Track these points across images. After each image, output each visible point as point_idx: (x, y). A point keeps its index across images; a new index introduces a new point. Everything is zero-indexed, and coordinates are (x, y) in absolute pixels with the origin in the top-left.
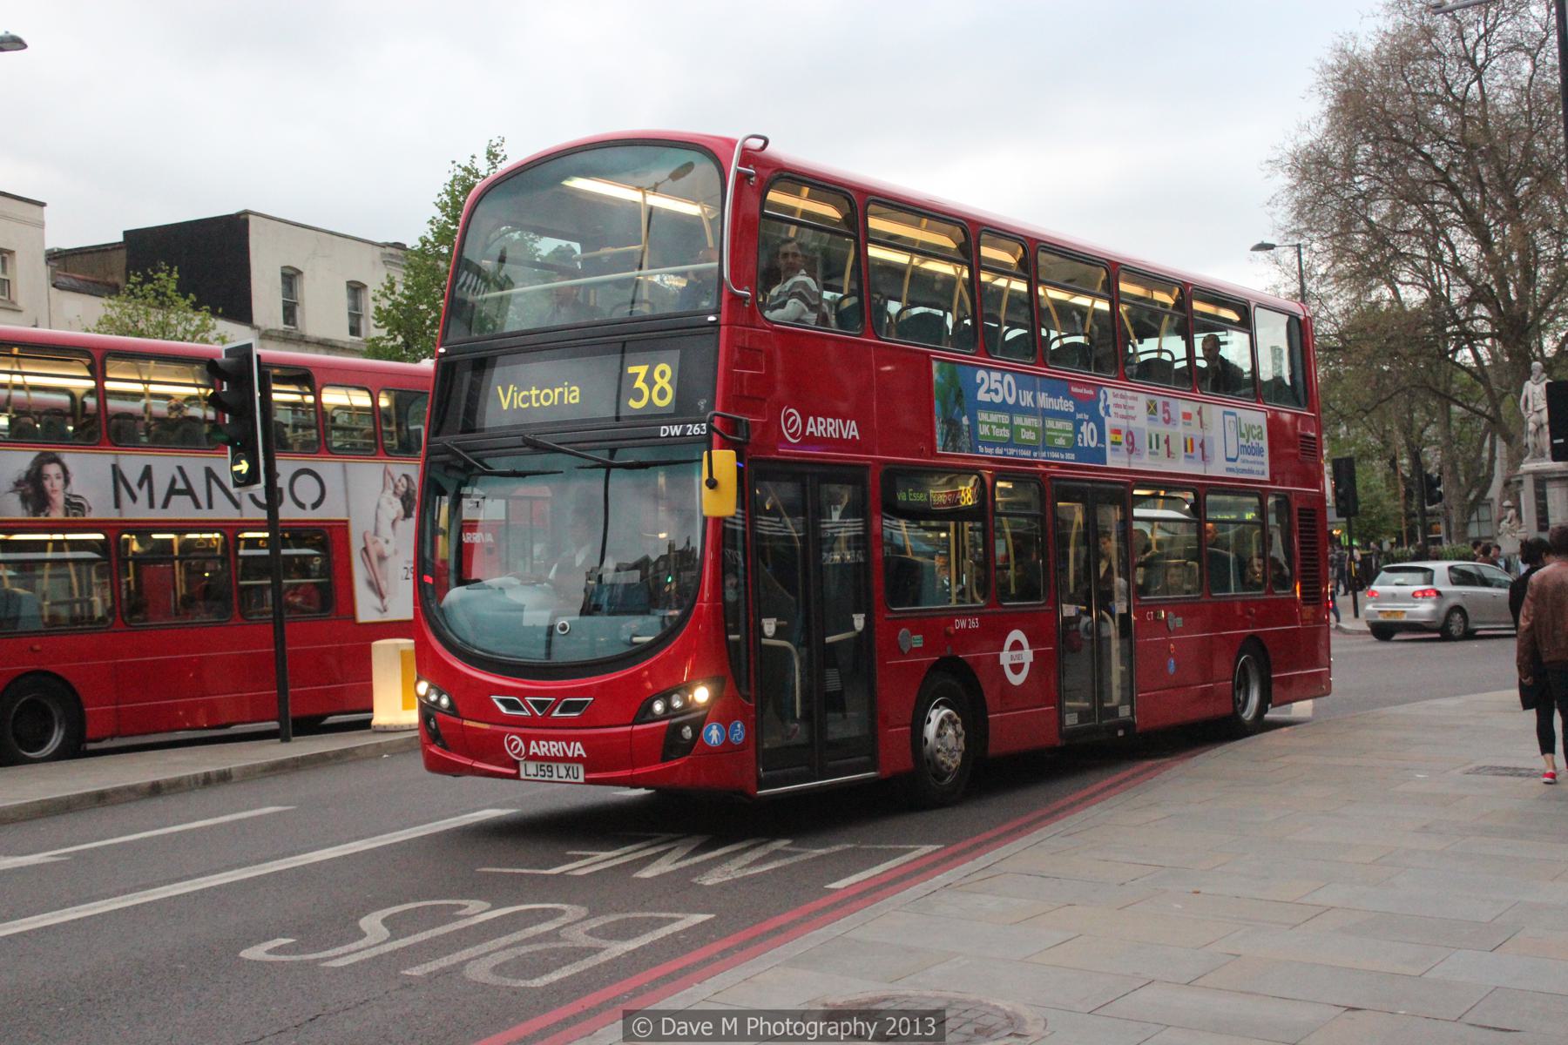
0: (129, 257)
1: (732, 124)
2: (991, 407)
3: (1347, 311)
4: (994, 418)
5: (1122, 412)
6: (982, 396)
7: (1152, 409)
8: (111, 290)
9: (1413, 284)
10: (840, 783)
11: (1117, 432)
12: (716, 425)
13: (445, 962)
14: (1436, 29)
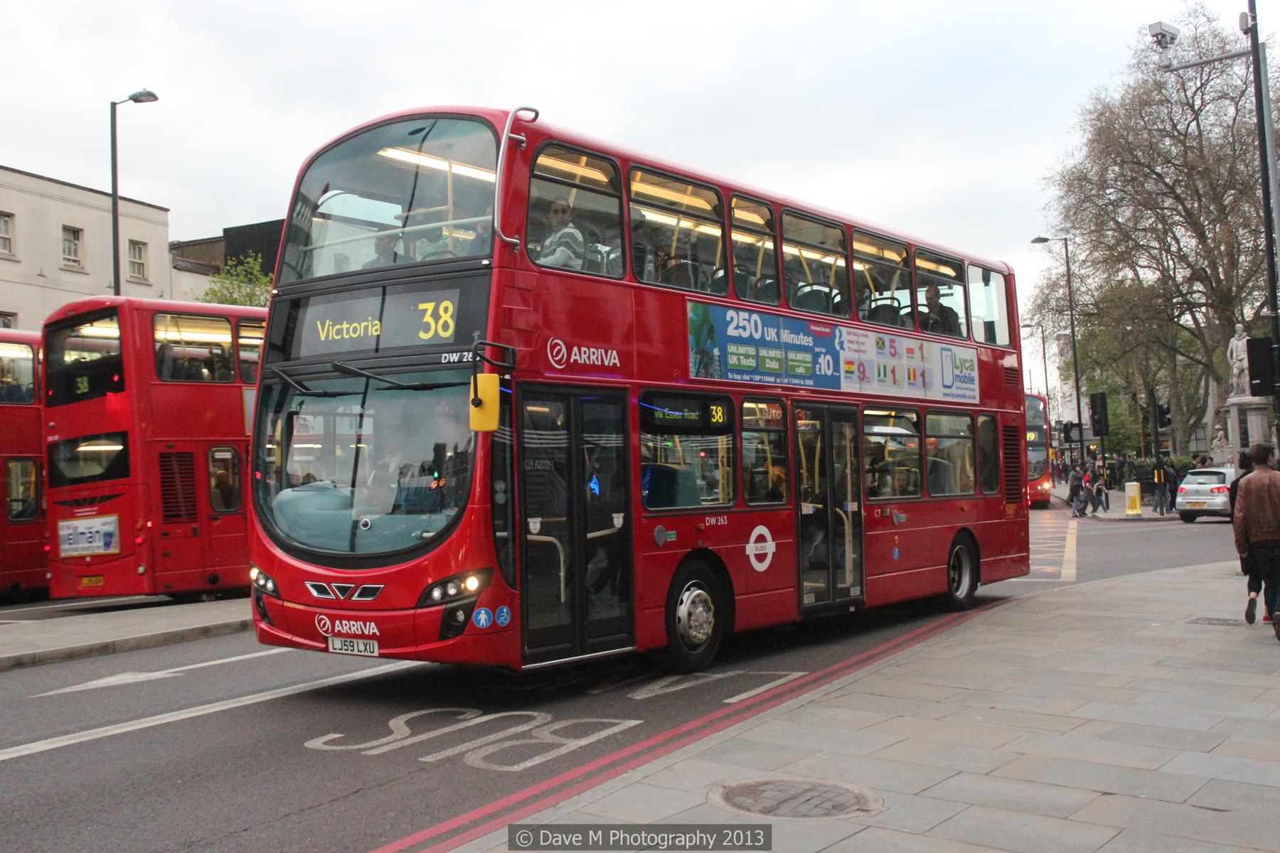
0: (227, 246)
1: (504, 97)
2: (739, 341)
3: (1101, 287)
4: (742, 350)
5: (855, 346)
6: (731, 331)
7: (880, 345)
8: (216, 271)
9: (1149, 267)
10: (615, 655)
11: (851, 363)
12: (487, 353)
13: (449, 752)
14: (1165, 83)
